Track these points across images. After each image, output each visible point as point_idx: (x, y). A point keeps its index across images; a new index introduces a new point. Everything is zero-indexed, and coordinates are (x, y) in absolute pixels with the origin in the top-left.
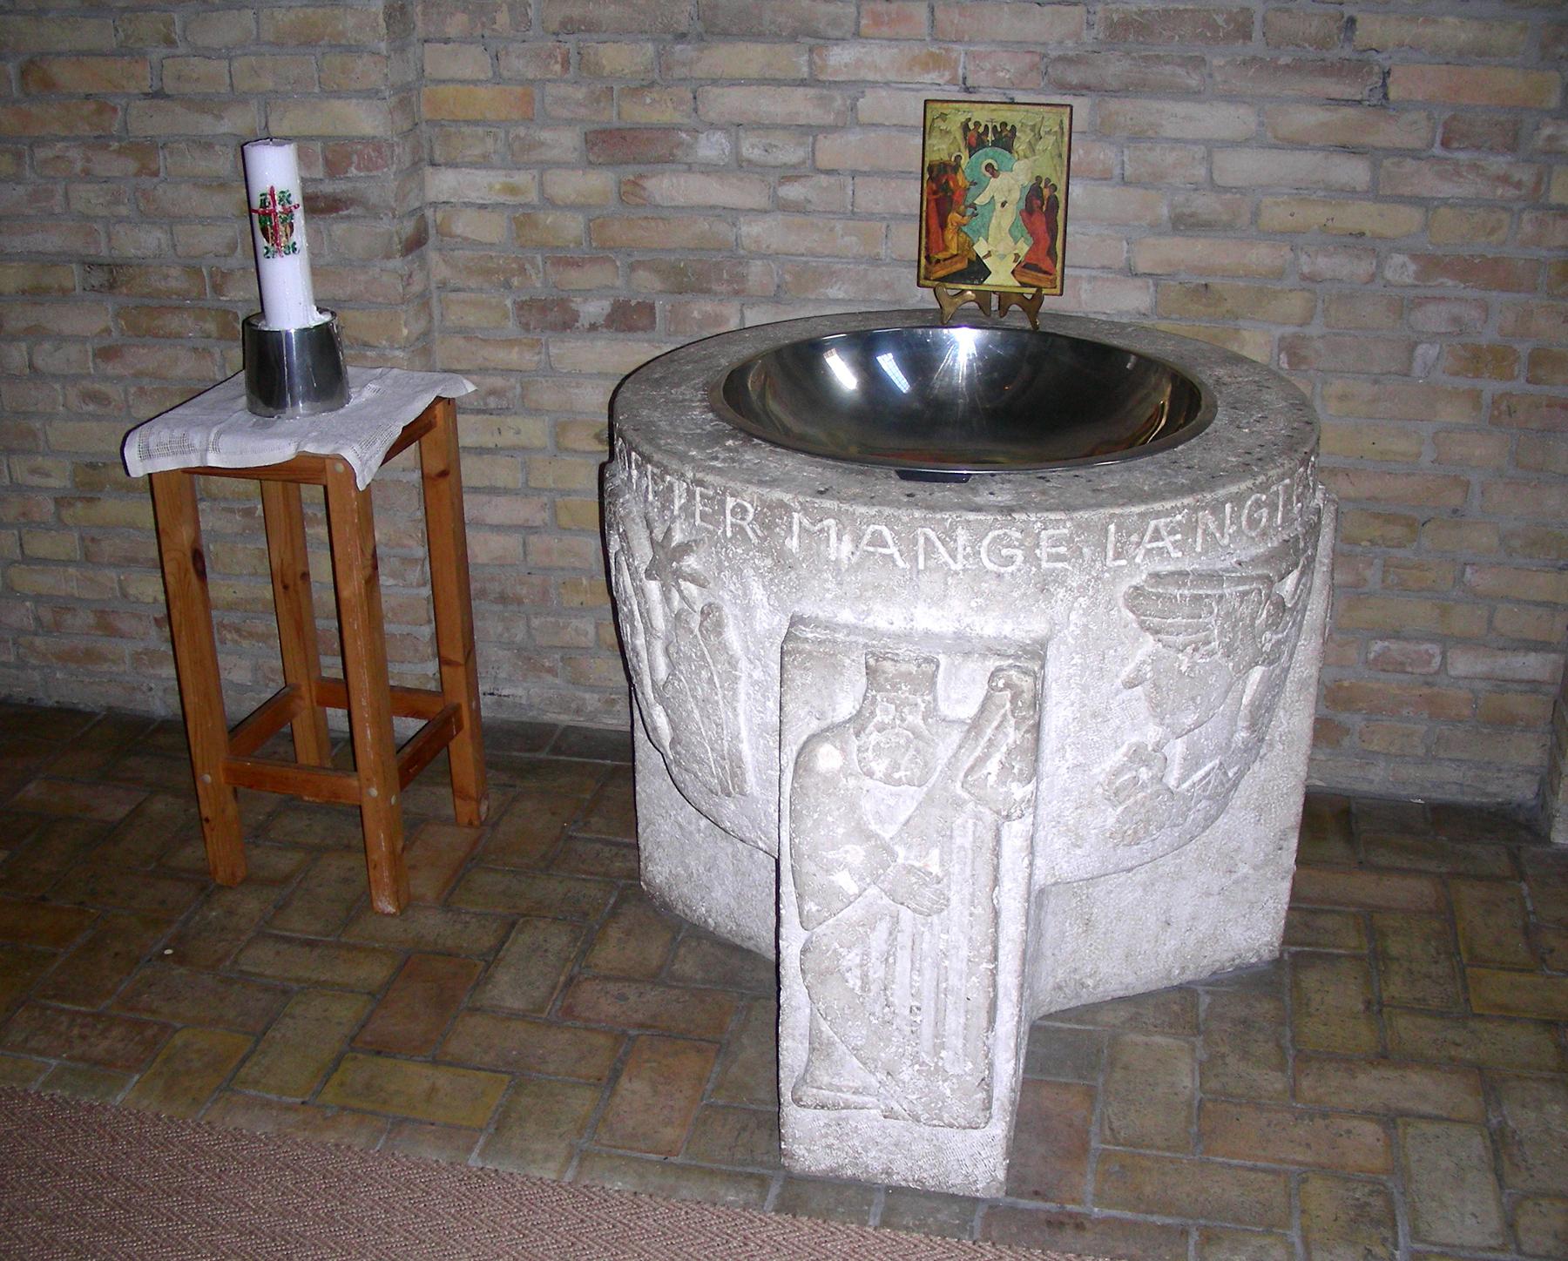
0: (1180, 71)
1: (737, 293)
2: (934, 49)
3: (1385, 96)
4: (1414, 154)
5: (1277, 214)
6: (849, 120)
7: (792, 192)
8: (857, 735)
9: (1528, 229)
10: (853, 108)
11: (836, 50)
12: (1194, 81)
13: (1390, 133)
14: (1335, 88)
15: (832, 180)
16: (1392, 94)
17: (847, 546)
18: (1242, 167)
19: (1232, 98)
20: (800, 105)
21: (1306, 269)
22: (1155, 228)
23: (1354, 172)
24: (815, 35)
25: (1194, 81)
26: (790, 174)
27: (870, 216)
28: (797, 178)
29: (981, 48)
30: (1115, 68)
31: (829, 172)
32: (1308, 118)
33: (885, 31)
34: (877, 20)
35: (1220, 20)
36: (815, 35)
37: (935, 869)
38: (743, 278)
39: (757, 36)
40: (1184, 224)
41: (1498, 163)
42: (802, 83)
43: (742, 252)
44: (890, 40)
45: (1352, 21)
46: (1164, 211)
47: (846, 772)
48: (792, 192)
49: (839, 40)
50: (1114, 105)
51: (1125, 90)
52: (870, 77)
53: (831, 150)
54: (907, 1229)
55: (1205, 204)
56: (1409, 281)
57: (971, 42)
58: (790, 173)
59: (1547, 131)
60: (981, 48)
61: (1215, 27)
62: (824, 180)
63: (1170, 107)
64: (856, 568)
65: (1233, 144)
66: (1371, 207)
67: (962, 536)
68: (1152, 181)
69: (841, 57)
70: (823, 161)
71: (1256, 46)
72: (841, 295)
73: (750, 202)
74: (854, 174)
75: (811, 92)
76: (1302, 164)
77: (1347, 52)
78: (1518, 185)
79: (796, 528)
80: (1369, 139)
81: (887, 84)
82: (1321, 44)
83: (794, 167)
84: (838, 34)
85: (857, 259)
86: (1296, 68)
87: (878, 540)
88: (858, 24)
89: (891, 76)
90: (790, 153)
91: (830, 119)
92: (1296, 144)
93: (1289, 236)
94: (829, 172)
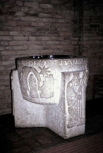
0: (43, 34)
1: (1, 60)
2: (21, 32)
3: (59, 36)
4: (62, 40)
5: (52, 47)
6: (13, 40)
7: (7, 48)
8: (74, 81)
9: (71, 47)
10: (13, 38)
11: (11, 32)
12: (44, 35)
13: (60, 39)
14: (56, 35)
15: (11, 46)
16: (60, 35)
17: (67, 63)
18: (49, 43)
19: (48, 36)
20: (8, 38)
21: (55, 52)
22: (42, 49)
23: (58, 42)
24: (9, 30)
25: (44, 35)
26: (7, 46)
27: (16, 50)
28: (7, 46)
29: (25, 32)
30: (38, 34)
31: (11, 46)
32: (54, 38)
33: (16, 30)
34: (15, 29)
35: (46, 29)
36: (9, 30)
37: (80, 94)
38: (2, 58)
39: (3, 30)
40: (45, 49)
41: (68, 41)
42: (8, 36)
43: (2, 55)
44: (17, 31)
45: (56, 29)
46: (43, 48)
47: (73, 86)
48: (7, 48)
49: (11, 31)
50: (38, 37)
51: (39, 36)
52: (15, 35)
53: (11, 43)
54: (80, 139)
55: (46, 47)
56: (63, 52)
57: (25, 31)
58: (7, 46)
59: (71, 38)
60: (25, 32)
61: (45, 29)
62: (11, 47)
63: (42, 37)
64: (68, 66)
65: (48, 40)
66: (59, 46)
67: (77, 61)
68: (41, 45)
69: (12, 33)
70: (10, 44)
71: (49, 31)
72: (13, 59)
73: (2, 49)
74: (13, 46)
75: (9, 37)
76: (53, 42)
77: (56, 32)
78: (70, 43)
79: (62, 62)
80: (59, 39)
81: (16, 36)
82: (54, 31)
83: (7, 45)
84: (11, 30)
85: (15, 55)
86: (53, 33)
87: (70, 62)
88: (13, 29)
89: (17, 35)
90: (7, 44)
91: (11, 40)
92: (53, 40)
93: (53, 49)
94: (11, 46)
